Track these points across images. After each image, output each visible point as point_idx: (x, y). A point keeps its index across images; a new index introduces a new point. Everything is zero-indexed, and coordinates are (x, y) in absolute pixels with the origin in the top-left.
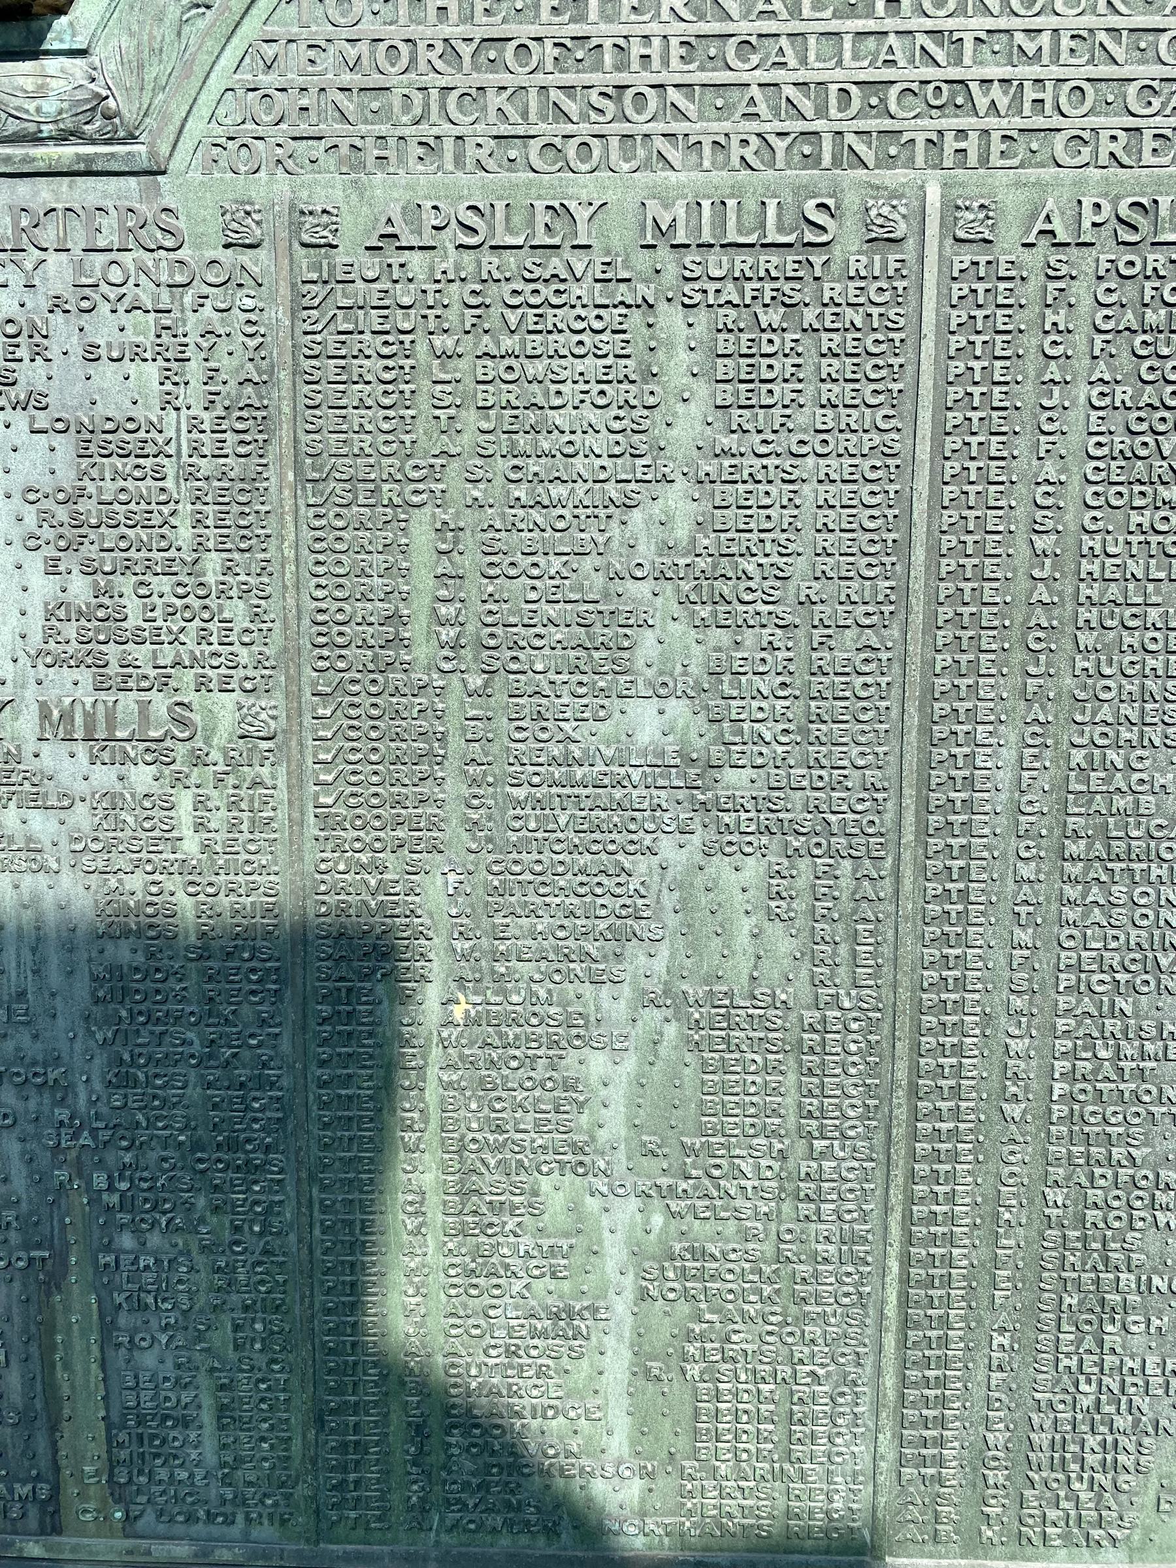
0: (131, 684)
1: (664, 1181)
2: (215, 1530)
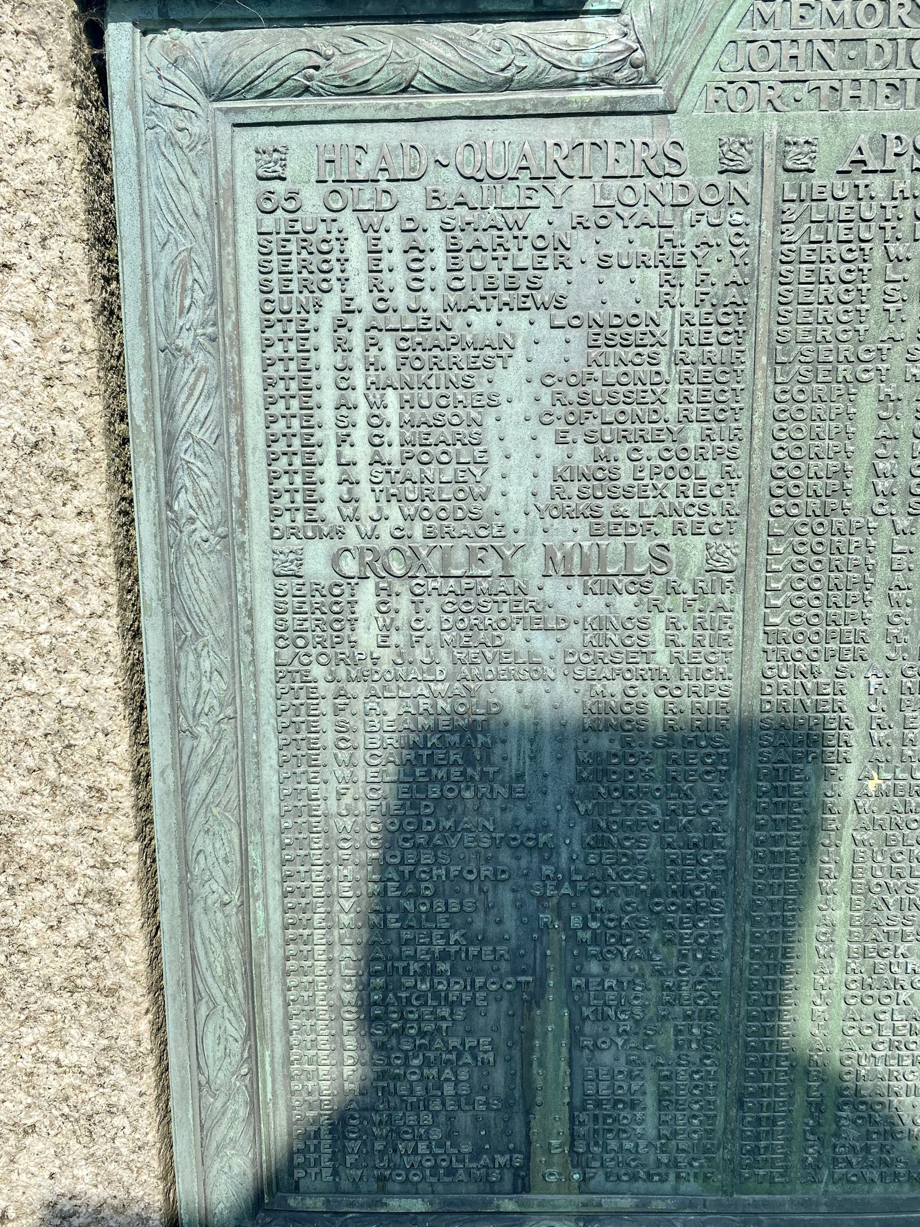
2: (651, 1187)
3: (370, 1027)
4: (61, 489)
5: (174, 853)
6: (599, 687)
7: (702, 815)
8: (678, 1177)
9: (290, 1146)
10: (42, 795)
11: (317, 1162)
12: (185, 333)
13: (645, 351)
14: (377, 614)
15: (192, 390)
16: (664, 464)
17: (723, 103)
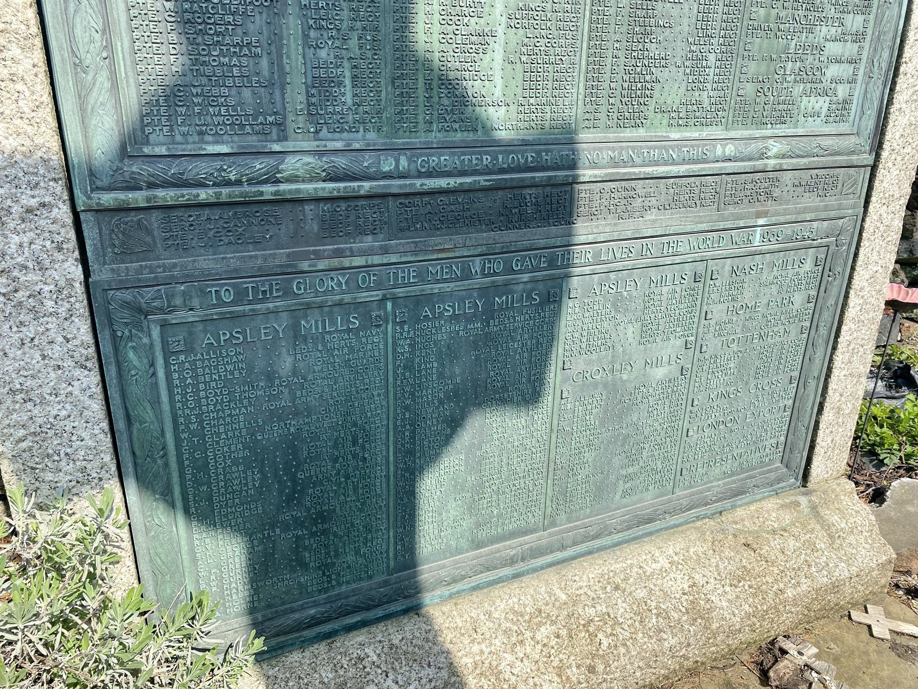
2: (352, 135)
9: (141, 111)
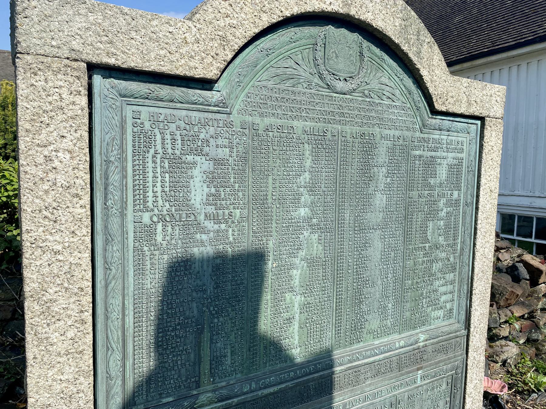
0: (222, 208)
1: (304, 291)
2: (230, 378)
3: (158, 349)
4: (75, 200)
5: (103, 305)
6: (217, 247)
7: (240, 277)
8: (236, 373)
9: (134, 391)
10: (62, 292)
11: (142, 393)
12: (112, 157)
13: (226, 167)
14: (162, 232)
15: (114, 172)
16: (231, 193)
17: (241, 113)
